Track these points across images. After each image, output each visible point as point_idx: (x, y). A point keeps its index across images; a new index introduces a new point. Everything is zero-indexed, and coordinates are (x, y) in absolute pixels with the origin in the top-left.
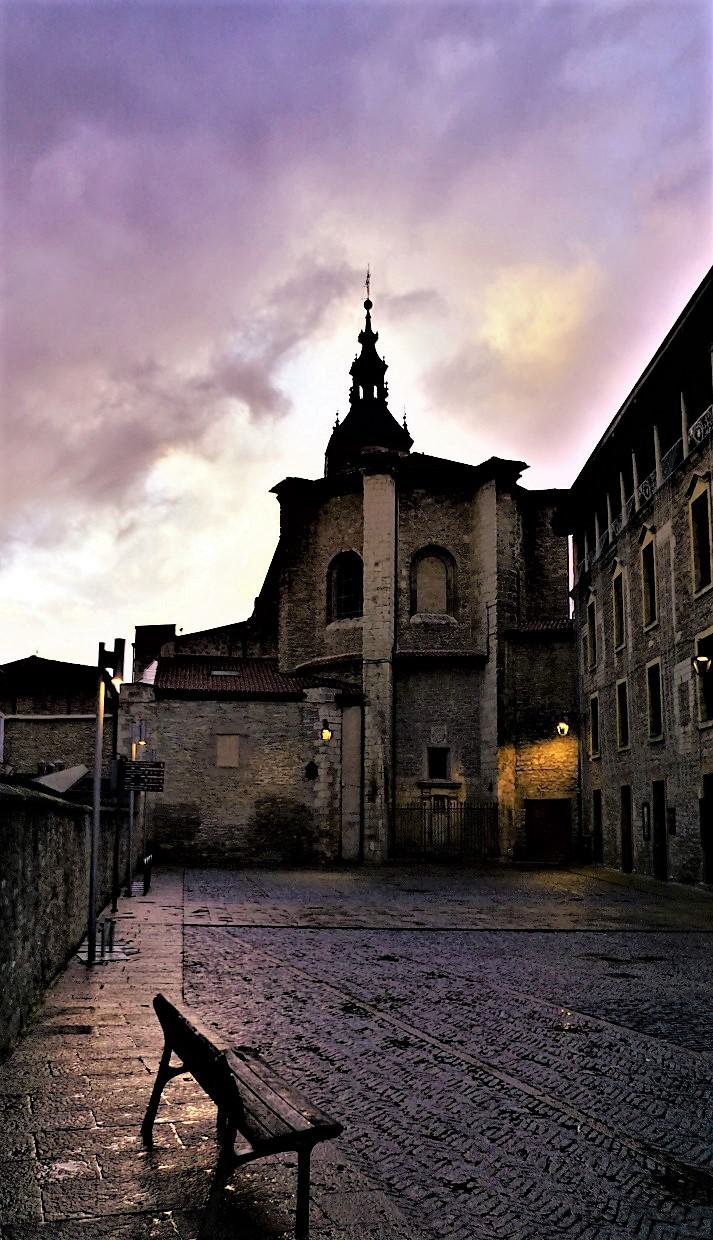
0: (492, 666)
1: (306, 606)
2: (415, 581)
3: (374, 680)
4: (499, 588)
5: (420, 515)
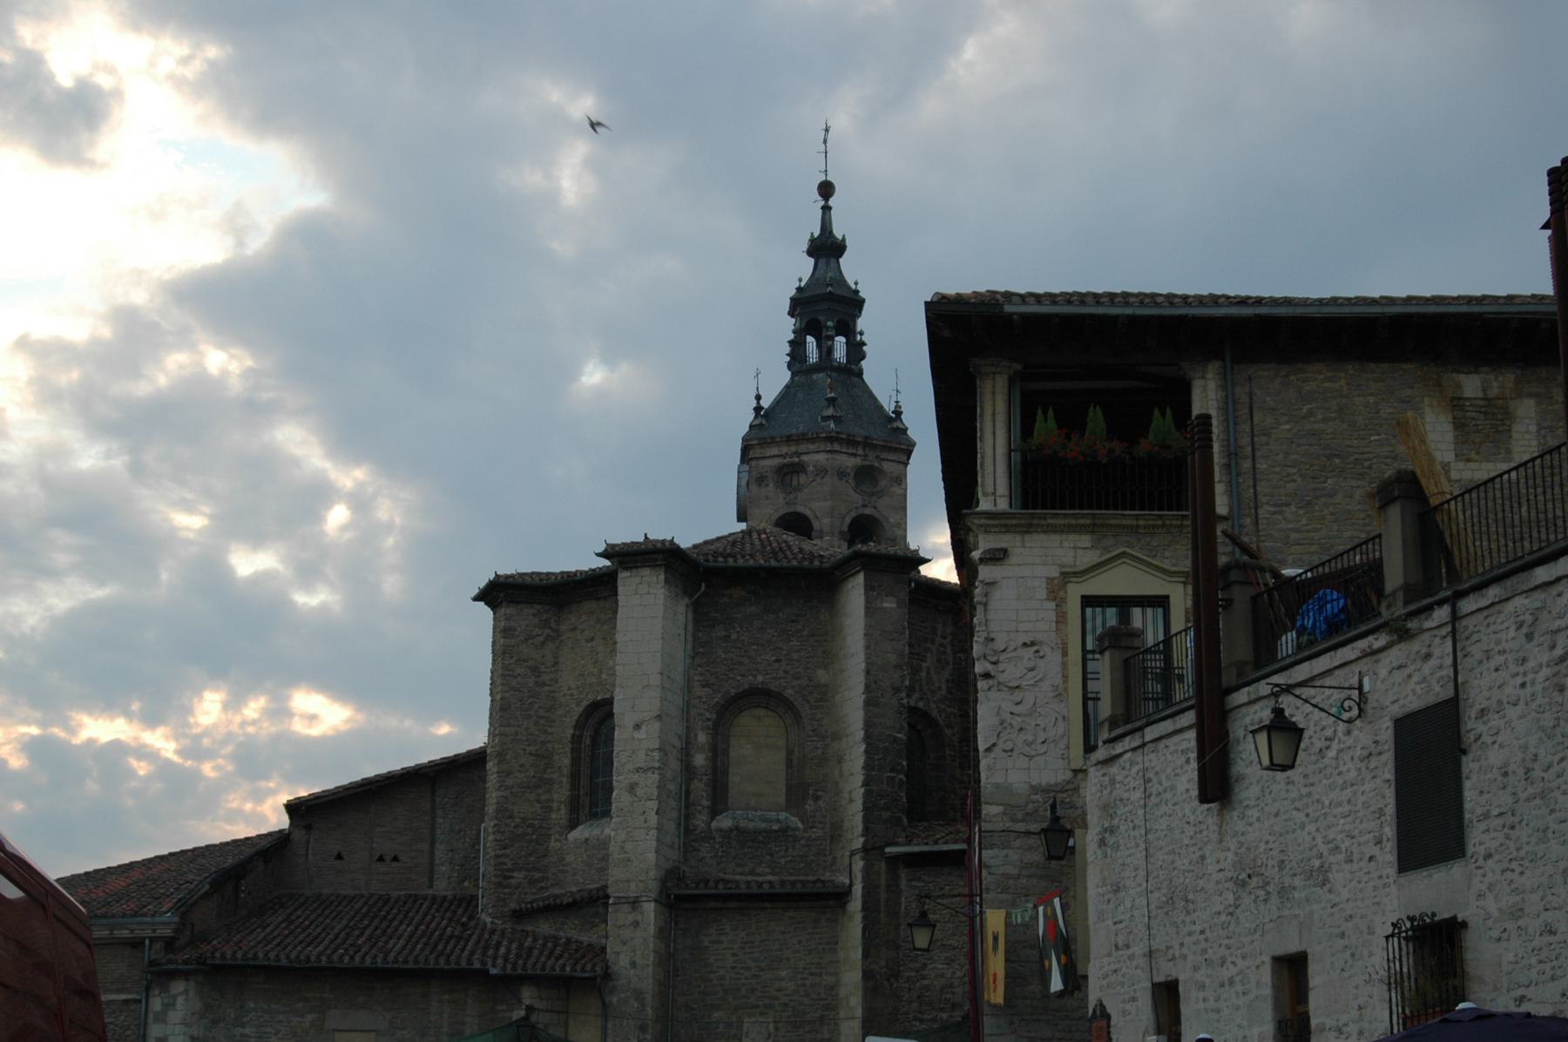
0: (856, 904)
1: (532, 797)
5: (734, 636)
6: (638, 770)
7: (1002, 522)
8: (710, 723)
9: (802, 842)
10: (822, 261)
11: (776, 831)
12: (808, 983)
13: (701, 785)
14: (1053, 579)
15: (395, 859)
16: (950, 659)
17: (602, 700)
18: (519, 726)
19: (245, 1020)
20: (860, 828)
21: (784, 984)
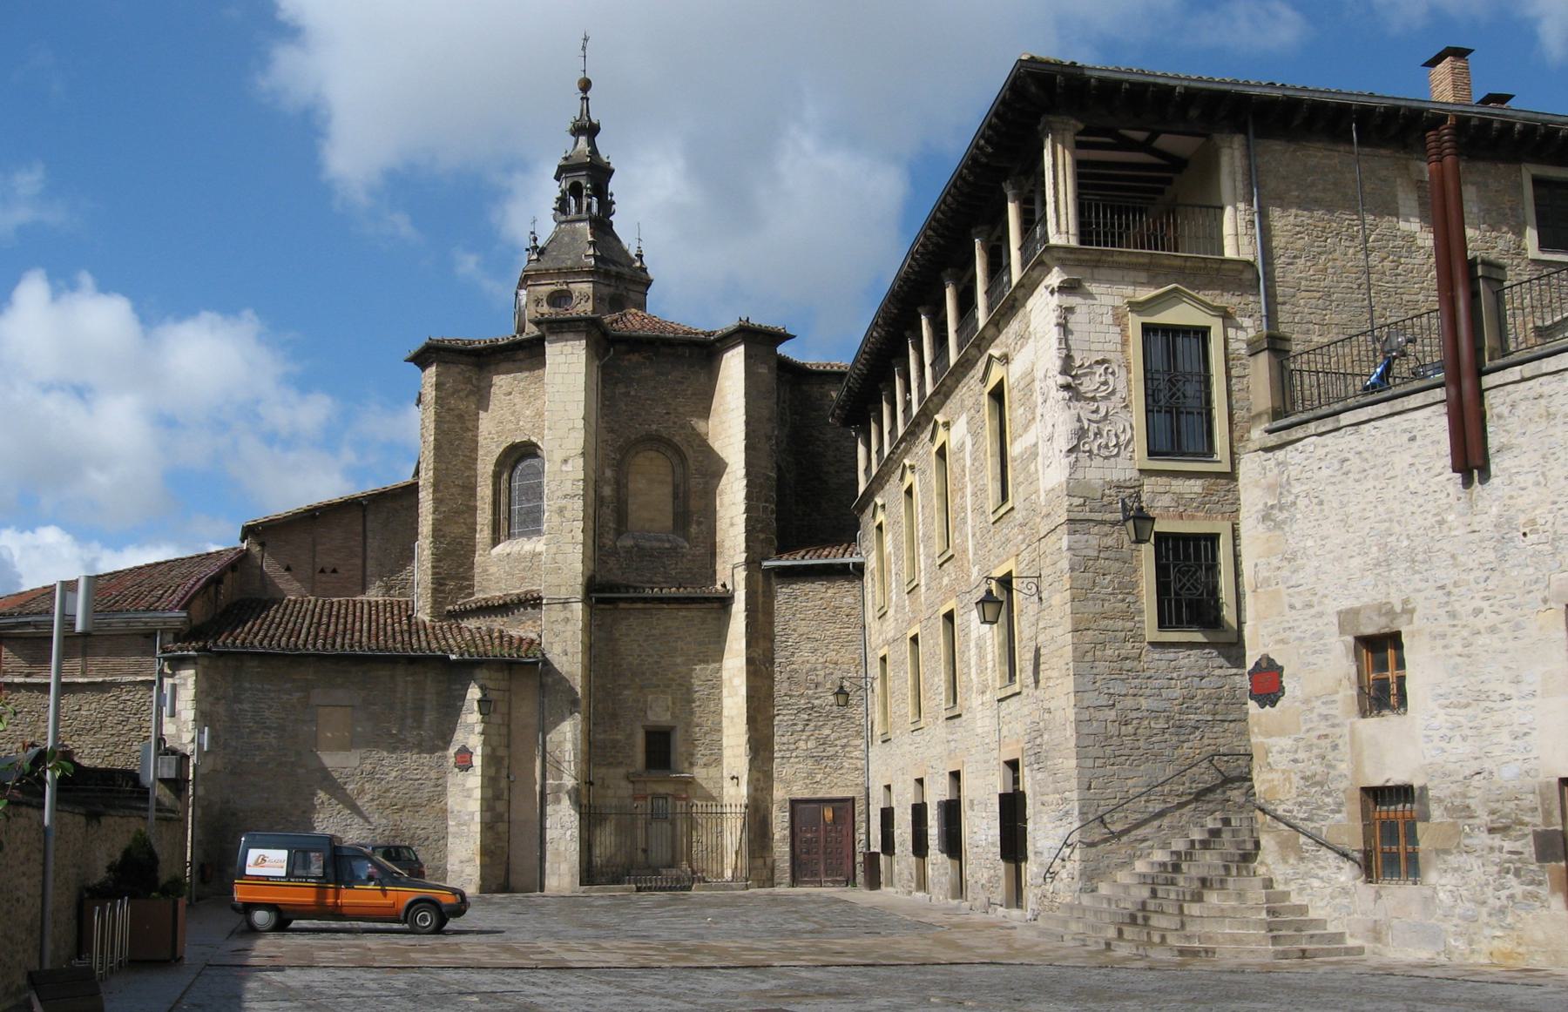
3: (559, 627)
5: (633, 393)
6: (566, 496)
7: (1076, 256)
11: (667, 549)
13: (609, 511)
14: (1117, 307)
15: (334, 571)
16: (789, 419)
19: (243, 697)
21: (679, 669)
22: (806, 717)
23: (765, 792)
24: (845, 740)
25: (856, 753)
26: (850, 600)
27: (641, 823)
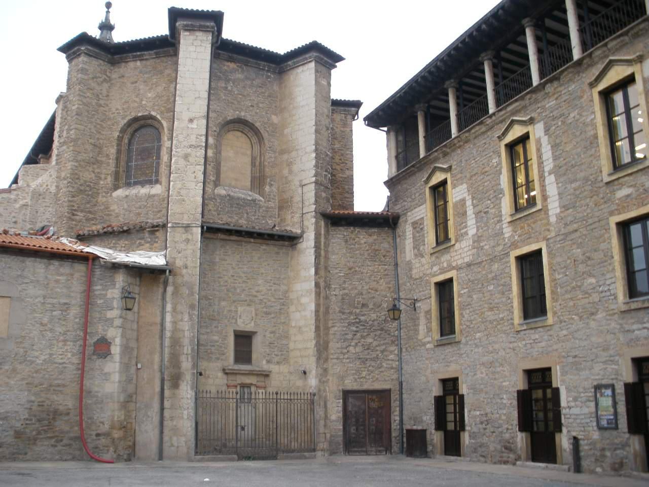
1: (91, 169)
2: (220, 153)
4: (316, 166)
5: (229, 88)
6: (191, 146)
8: (216, 133)
9: (264, 208)
10: (105, 32)
12: (273, 288)
17: (142, 116)
18: (86, 126)
20: (313, 200)
22: (354, 329)
23: (325, 384)
24: (384, 347)
25: (392, 357)
26: (386, 245)
27: (232, 404)
